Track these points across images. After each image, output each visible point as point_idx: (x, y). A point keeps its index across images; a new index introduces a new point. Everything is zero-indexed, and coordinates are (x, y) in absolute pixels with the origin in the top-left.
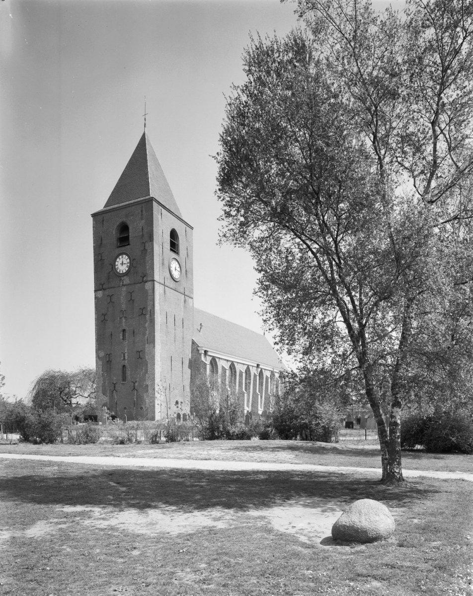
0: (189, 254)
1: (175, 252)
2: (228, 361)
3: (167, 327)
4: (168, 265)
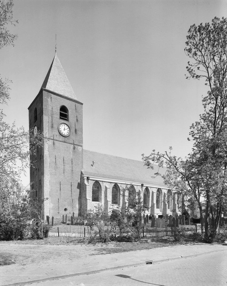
0: (79, 119)
1: (66, 120)
2: (111, 183)
3: (56, 164)
4: (57, 127)
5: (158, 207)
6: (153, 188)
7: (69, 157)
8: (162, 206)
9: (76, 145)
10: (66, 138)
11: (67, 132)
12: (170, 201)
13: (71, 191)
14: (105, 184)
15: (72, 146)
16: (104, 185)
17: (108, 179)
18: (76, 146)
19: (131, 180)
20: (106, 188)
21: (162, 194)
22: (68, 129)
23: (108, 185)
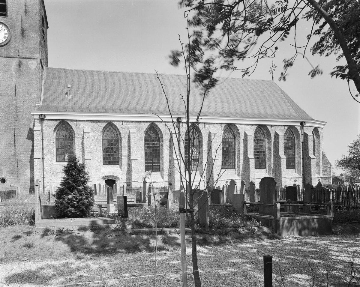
5: (290, 165)
6: (211, 125)
7: (9, 83)
8: (240, 162)
9: (23, 58)
10: (3, 48)
11: (3, 36)
12: (267, 150)
13: (15, 146)
14: (82, 124)
15: (15, 62)
16: (80, 127)
17: (255, 119)
18: (24, 61)
19: (259, 116)
20: (277, 135)
21: (240, 137)
22: (6, 32)
23: (87, 128)
